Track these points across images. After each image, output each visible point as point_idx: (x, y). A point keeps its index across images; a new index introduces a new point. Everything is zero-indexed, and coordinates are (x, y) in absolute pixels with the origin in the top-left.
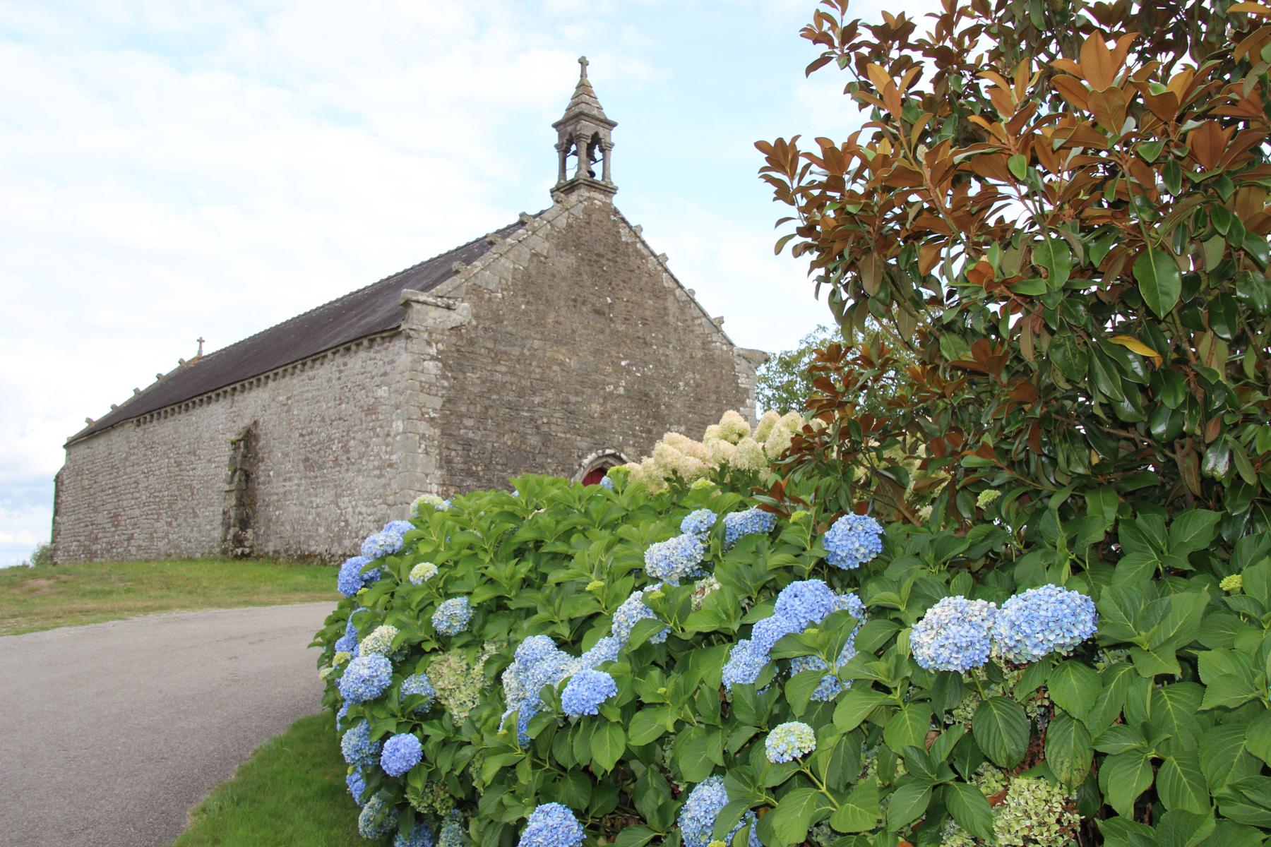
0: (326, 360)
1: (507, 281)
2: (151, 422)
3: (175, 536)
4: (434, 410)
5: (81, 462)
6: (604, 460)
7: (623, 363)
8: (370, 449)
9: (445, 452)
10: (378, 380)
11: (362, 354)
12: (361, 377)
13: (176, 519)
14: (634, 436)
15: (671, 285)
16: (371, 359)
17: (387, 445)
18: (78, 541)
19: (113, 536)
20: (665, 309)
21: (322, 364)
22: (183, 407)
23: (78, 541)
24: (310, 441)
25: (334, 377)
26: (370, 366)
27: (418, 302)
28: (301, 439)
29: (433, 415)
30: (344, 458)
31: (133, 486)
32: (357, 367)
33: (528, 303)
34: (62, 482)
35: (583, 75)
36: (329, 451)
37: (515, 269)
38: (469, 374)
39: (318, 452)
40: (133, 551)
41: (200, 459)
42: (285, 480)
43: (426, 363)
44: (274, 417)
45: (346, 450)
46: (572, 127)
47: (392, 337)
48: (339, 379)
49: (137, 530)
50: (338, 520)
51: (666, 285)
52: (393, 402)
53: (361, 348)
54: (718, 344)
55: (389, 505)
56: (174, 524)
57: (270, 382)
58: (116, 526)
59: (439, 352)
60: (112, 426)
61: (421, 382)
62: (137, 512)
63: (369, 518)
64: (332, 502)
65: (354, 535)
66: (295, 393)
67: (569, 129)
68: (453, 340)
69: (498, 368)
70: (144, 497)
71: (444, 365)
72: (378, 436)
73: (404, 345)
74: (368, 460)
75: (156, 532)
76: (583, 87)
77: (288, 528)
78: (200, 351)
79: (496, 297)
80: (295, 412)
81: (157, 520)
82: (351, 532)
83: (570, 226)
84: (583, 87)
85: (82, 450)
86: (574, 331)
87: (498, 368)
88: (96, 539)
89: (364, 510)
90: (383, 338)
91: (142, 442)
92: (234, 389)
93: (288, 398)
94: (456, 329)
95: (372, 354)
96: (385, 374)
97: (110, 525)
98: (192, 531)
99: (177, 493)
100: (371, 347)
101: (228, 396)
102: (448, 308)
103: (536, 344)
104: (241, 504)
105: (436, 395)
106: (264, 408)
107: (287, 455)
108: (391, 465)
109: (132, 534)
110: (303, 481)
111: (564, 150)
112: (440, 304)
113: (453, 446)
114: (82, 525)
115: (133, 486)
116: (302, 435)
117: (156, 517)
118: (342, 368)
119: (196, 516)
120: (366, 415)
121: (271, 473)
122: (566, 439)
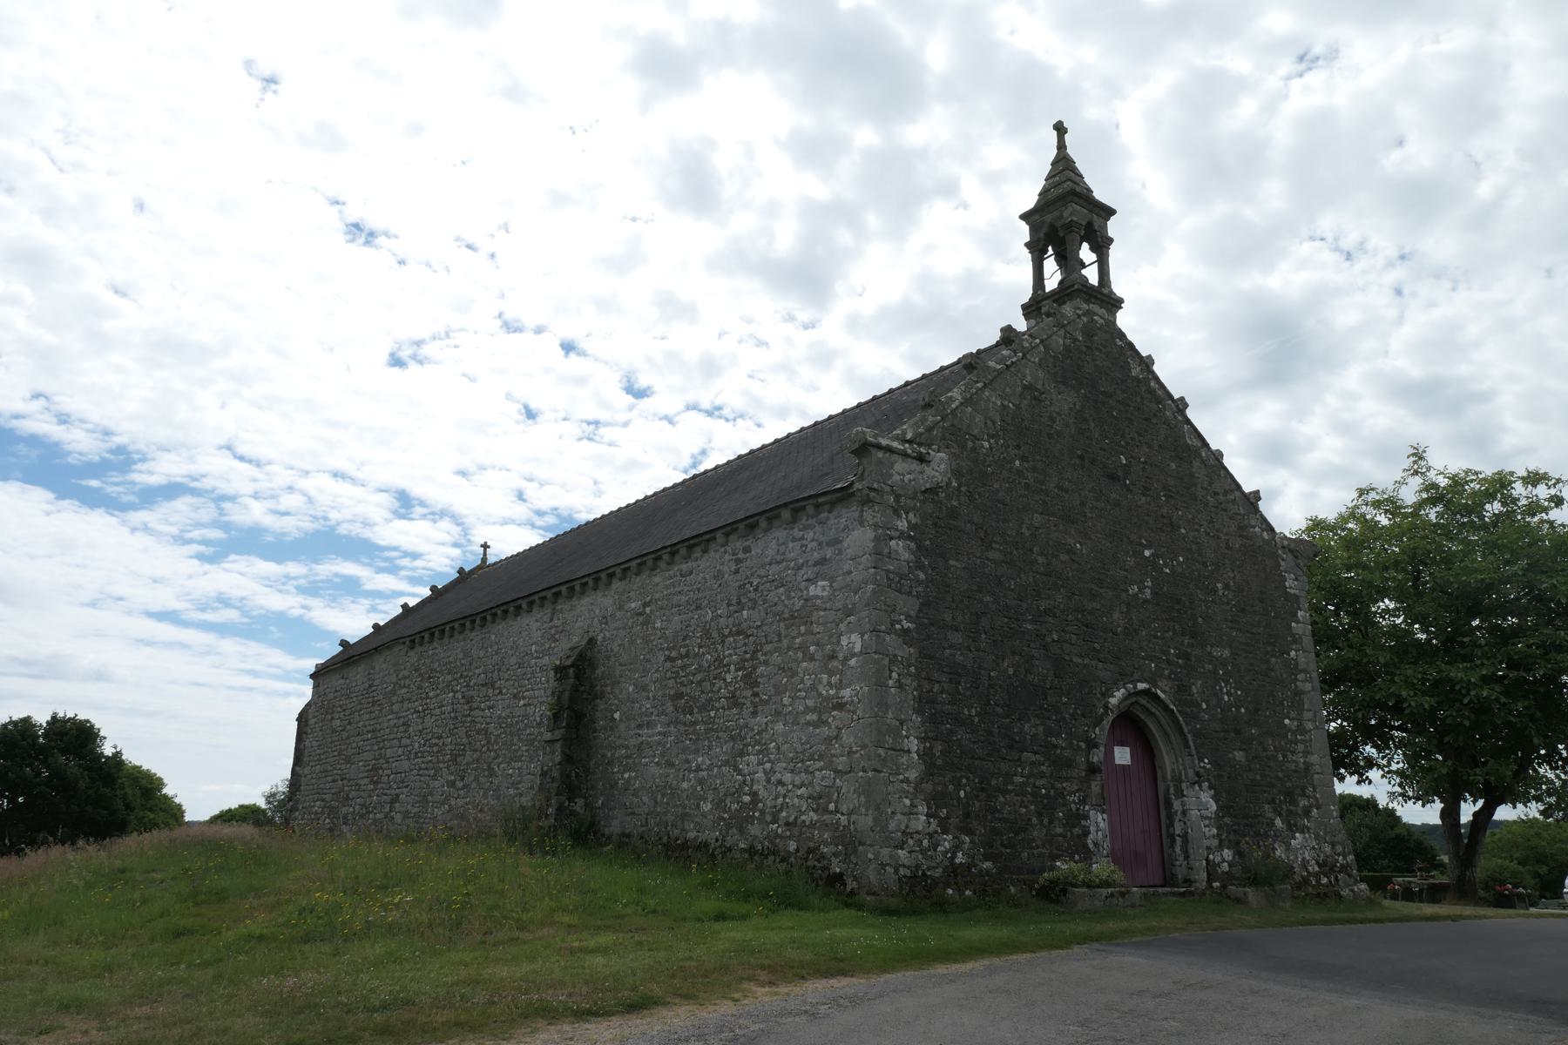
0: (713, 545)
1: (994, 422)
2: (431, 642)
3: (460, 802)
4: (908, 617)
5: (332, 696)
6: (1134, 699)
7: (1147, 553)
8: (797, 679)
9: (926, 686)
10: (809, 572)
11: (779, 534)
12: (775, 568)
13: (462, 779)
14: (1169, 662)
15: (1196, 443)
16: (794, 540)
17: (831, 673)
18: (323, 800)
19: (370, 796)
20: (1192, 476)
21: (705, 551)
22: (478, 622)
23: (323, 800)
24: (683, 667)
25: (726, 568)
26: (793, 552)
27: (879, 447)
28: (668, 664)
29: (906, 625)
30: (748, 693)
31: (402, 729)
32: (770, 552)
33: (1023, 458)
34: (307, 721)
35: (1061, 146)
36: (719, 683)
37: (1004, 407)
38: (952, 562)
39: (700, 683)
40: (398, 818)
41: (501, 693)
42: (640, 726)
43: (893, 543)
44: (622, 632)
45: (750, 681)
46: (1056, 214)
47: (833, 504)
48: (737, 571)
49: (405, 790)
50: (739, 791)
51: (1189, 442)
52: (839, 605)
53: (776, 523)
54: (1257, 529)
55: (837, 772)
56: (460, 784)
57: (535, 609)
58: (376, 783)
59: (911, 526)
60: (376, 649)
61: (888, 571)
62: (406, 765)
63: (799, 792)
64: (726, 763)
65: (769, 818)
66: (657, 596)
67: (1048, 218)
68: (929, 507)
69: (991, 555)
70: (417, 745)
71: (919, 547)
72: (812, 659)
73: (856, 514)
74: (793, 698)
75: (431, 794)
76: (1063, 167)
77: (645, 799)
78: (484, 559)
79: (983, 447)
80: (658, 625)
81: (434, 778)
82: (762, 812)
83: (1067, 349)
84: (1063, 167)
85: (336, 682)
86: (1083, 504)
87: (991, 555)
88: (347, 799)
89: (787, 777)
90: (817, 506)
91: (416, 670)
92: (557, 595)
93: (645, 605)
94: (933, 490)
95: (797, 533)
96: (822, 561)
97: (366, 781)
98: (485, 796)
99: (465, 740)
100: (794, 521)
101: (547, 604)
102: (921, 459)
103: (1037, 518)
104: (568, 759)
105: (910, 593)
106: (605, 620)
107: (645, 688)
108: (840, 706)
109: (397, 795)
110: (672, 728)
111: (1037, 249)
112: (909, 451)
113: (936, 676)
114: (330, 779)
115: (402, 729)
116: (669, 659)
117: (432, 772)
118: (741, 555)
119: (492, 773)
120: (787, 628)
121: (617, 715)
122: (1085, 666)
